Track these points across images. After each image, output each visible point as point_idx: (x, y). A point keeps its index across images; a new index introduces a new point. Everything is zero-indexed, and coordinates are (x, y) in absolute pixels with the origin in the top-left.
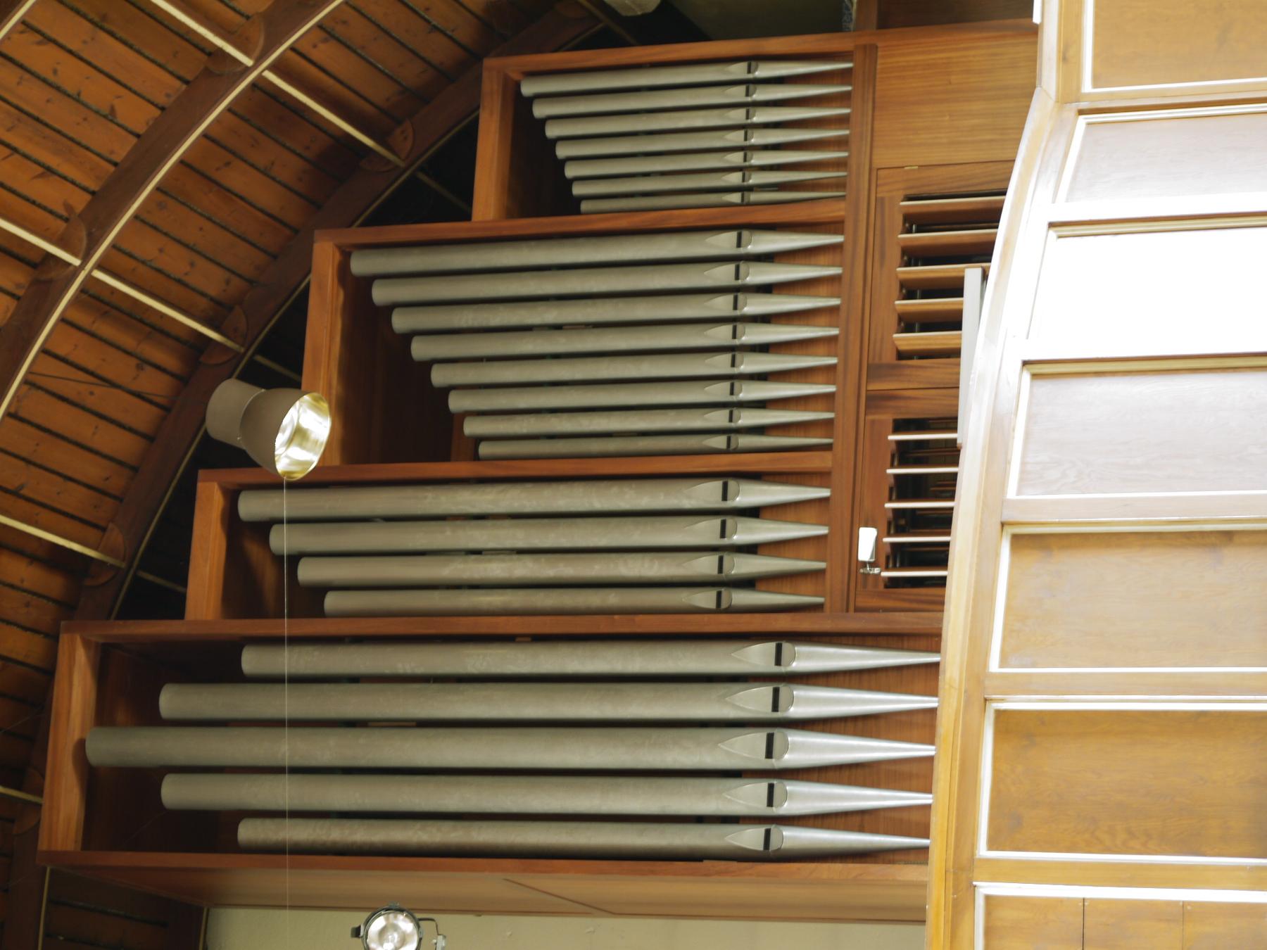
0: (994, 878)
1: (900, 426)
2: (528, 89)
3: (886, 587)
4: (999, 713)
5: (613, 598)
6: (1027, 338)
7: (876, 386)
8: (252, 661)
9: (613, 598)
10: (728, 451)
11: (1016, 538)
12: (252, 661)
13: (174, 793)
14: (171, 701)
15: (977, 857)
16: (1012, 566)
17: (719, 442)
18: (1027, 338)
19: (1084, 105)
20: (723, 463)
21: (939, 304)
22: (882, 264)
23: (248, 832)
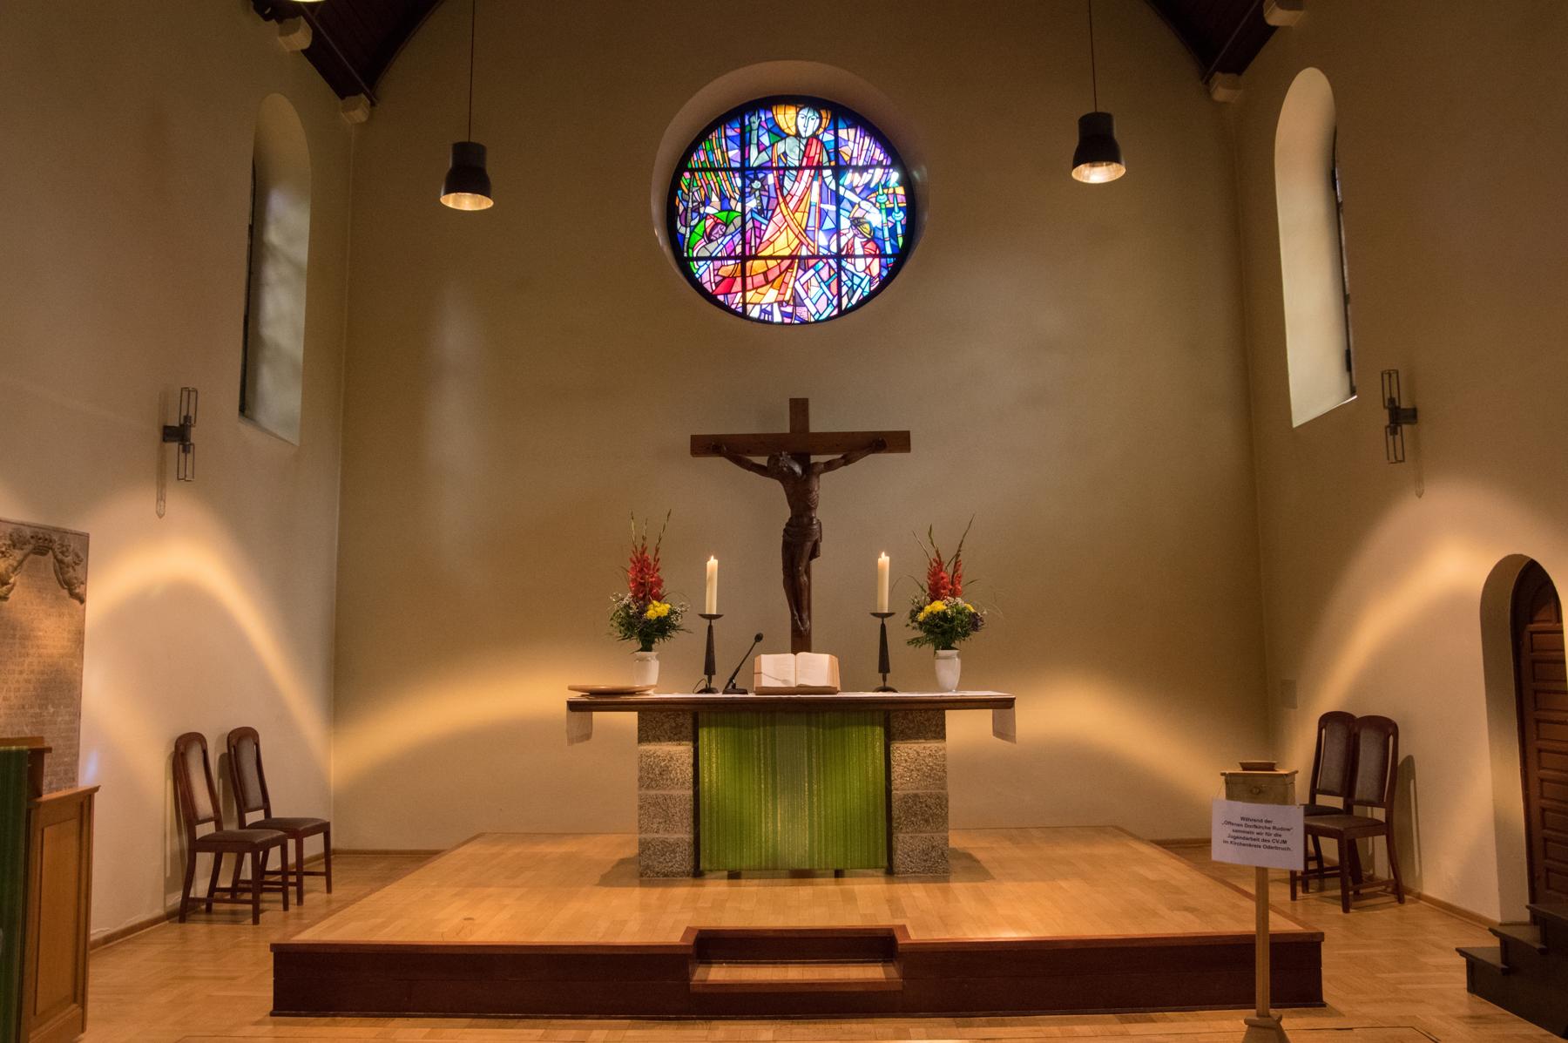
7: (18, 655)
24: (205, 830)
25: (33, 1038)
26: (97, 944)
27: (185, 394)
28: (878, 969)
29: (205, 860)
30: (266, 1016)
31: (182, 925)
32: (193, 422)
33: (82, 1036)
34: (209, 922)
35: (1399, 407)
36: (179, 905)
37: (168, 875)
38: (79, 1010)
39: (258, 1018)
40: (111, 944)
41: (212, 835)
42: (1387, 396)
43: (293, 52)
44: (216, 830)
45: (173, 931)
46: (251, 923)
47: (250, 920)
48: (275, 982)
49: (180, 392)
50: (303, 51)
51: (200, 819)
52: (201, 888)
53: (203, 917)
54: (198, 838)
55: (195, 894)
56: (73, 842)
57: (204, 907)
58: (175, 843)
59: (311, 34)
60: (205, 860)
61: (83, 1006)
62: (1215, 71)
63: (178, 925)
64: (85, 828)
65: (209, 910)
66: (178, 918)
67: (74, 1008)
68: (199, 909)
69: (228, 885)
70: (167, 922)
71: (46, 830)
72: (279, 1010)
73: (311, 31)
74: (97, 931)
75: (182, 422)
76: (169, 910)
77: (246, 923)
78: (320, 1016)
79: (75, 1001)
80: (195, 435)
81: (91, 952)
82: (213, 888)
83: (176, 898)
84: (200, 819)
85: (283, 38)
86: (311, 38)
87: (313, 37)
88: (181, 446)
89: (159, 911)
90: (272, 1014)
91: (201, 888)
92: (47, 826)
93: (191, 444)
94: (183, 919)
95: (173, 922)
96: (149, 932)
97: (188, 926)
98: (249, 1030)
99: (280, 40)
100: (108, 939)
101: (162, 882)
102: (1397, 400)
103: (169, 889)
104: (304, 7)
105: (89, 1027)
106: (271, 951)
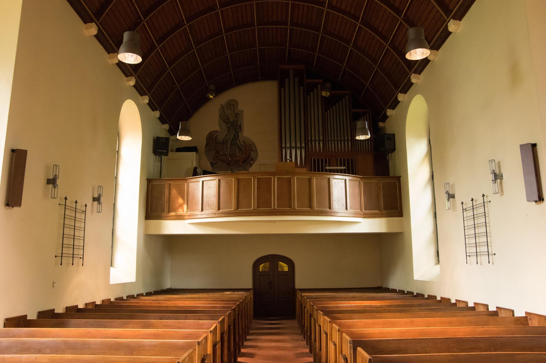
0: (273, 179)
1: (329, 159)
2: (368, 114)
3: (118, 64)
4: (291, 178)
5: (309, 128)
6: (477, 264)
7: (333, 156)
8: (301, 87)
9: (309, 128)
10: (326, 140)
11: (310, 178)
12: (301, 87)
13: (287, 80)
14: (296, 79)
15: (331, 177)
16: (307, 178)
17: (327, 139)
18: (477, 264)
19: (360, 181)
20: (325, 140)
21: (219, 333)
22: (234, 320)
23: (282, 89)
27: (55, 167)
28: (251, 287)
32: (58, 177)
35: (449, 193)
42: (56, 189)
43: (113, 64)
44: (38, 318)
49: (52, 167)
50: (133, 86)
59: (97, 29)
62: (387, 109)
73: (97, 28)
75: (54, 177)
80: (58, 182)
85: (110, 60)
86: (97, 31)
87: (98, 31)
88: (53, 186)
93: (57, 185)
99: (109, 60)
102: (53, 187)
104: (127, 65)
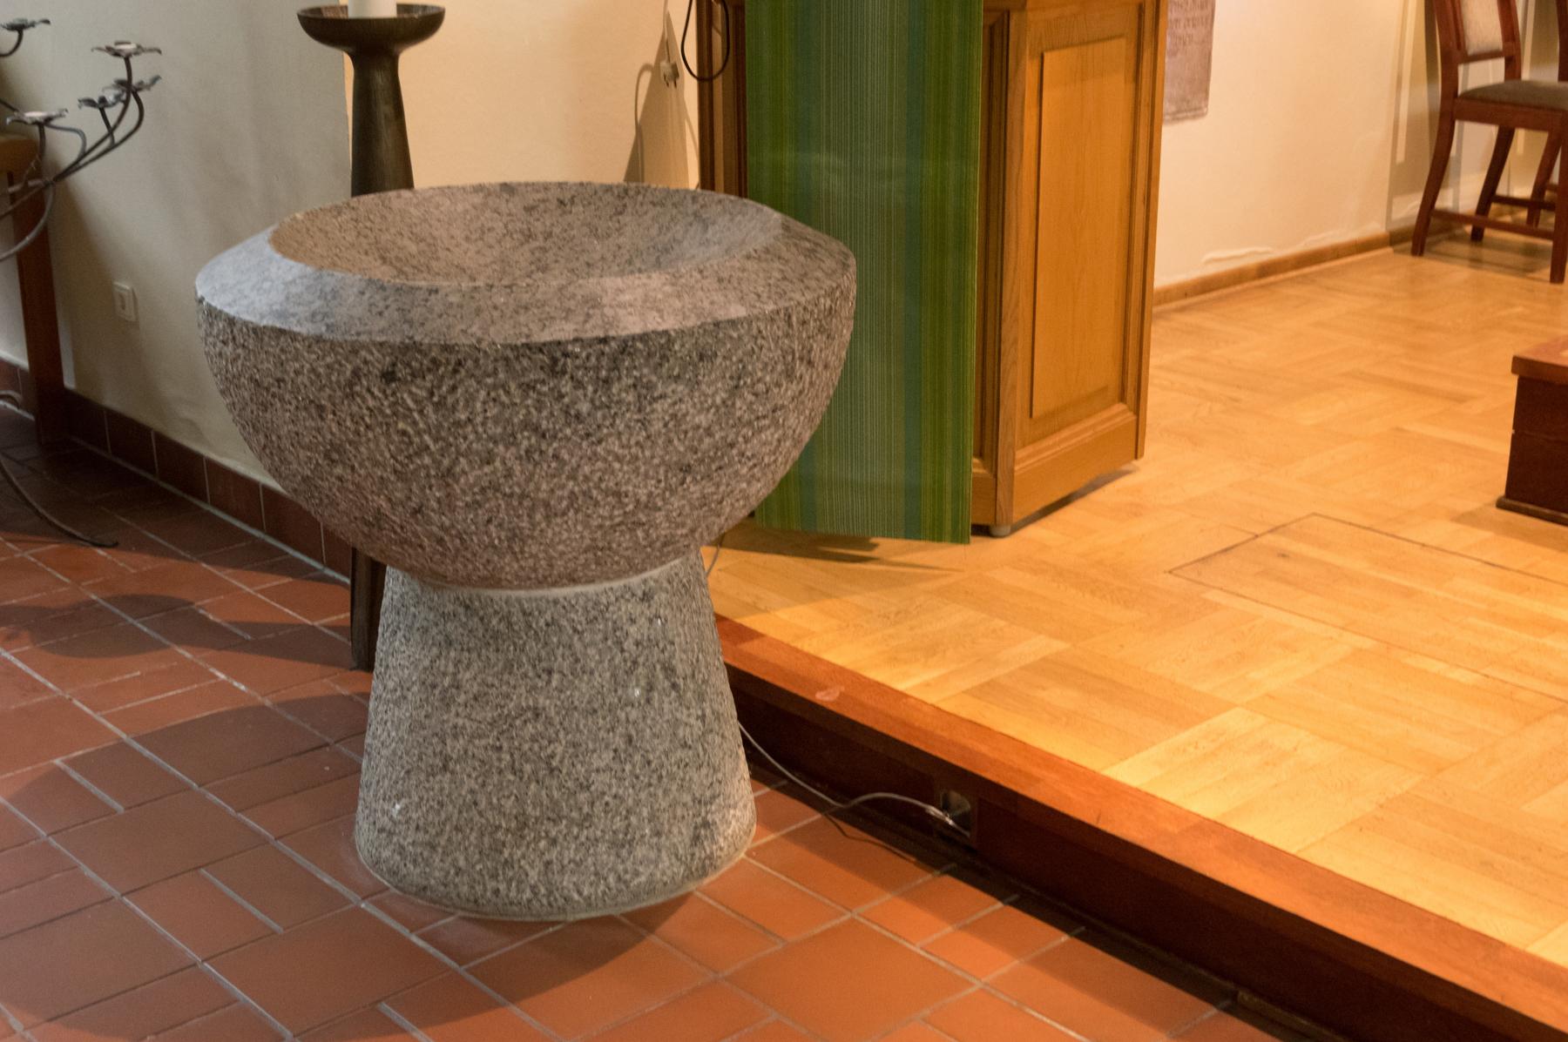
24: (1484, 75)
25: (1023, 460)
26: (1169, 295)
29: (1476, 140)
30: (1490, 505)
31: (1417, 260)
33: (1135, 463)
34: (1476, 262)
36: (1414, 222)
37: (1400, 157)
38: (1130, 417)
39: (1471, 505)
40: (1272, 279)
41: (1495, 88)
45: (1403, 263)
46: (1548, 278)
47: (1546, 272)
48: (1514, 437)
51: (1471, 52)
52: (1462, 194)
53: (1464, 249)
54: (1460, 92)
55: (1456, 200)
56: (1117, 87)
57: (1469, 229)
58: (1421, 98)
60: (1476, 140)
61: (1138, 408)
63: (1409, 259)
64: (1147, 55)
65: (1477, 236)
66: (1409, 245)
67: (1119, 413)
68: (1458, 232)
69: (1523, 190)
70: (1389, 250)
71: (1047, 57)
72: (1514, 499)
74: (1169, 270)
76: (1395, 227)
77: (1536, 275)
78: (1173, 805)
79: (1122, 399)
81: (1156, 310)
82: (1489, 194)
83: (1409, 208)
84: (1471, 52)
89: (1376, 227)
90: (1501, 505)
91: (1462, 194)
92: (1053, 48)
94: (1419, 250)
95: (1403, 252)
96: (1351, 265)
97: (1427, 265)
98: (1440, 532)
100: (1206, 288)
101: (1386, 174)
103: (1397, 188)
105: (1150, 448)
106: (1514, 371)
